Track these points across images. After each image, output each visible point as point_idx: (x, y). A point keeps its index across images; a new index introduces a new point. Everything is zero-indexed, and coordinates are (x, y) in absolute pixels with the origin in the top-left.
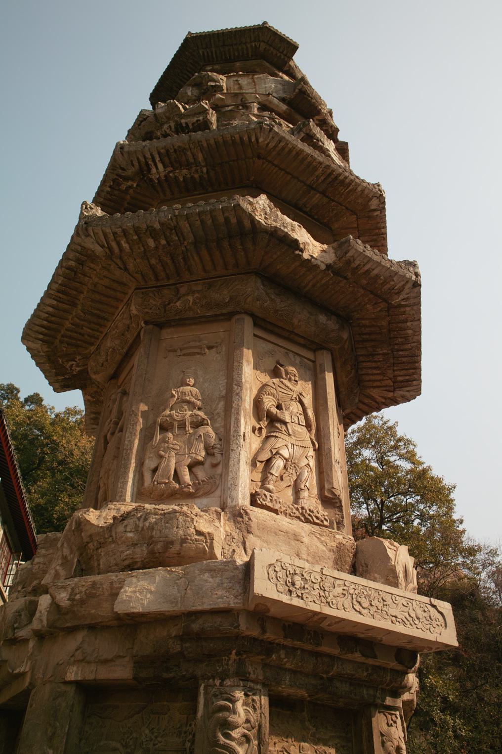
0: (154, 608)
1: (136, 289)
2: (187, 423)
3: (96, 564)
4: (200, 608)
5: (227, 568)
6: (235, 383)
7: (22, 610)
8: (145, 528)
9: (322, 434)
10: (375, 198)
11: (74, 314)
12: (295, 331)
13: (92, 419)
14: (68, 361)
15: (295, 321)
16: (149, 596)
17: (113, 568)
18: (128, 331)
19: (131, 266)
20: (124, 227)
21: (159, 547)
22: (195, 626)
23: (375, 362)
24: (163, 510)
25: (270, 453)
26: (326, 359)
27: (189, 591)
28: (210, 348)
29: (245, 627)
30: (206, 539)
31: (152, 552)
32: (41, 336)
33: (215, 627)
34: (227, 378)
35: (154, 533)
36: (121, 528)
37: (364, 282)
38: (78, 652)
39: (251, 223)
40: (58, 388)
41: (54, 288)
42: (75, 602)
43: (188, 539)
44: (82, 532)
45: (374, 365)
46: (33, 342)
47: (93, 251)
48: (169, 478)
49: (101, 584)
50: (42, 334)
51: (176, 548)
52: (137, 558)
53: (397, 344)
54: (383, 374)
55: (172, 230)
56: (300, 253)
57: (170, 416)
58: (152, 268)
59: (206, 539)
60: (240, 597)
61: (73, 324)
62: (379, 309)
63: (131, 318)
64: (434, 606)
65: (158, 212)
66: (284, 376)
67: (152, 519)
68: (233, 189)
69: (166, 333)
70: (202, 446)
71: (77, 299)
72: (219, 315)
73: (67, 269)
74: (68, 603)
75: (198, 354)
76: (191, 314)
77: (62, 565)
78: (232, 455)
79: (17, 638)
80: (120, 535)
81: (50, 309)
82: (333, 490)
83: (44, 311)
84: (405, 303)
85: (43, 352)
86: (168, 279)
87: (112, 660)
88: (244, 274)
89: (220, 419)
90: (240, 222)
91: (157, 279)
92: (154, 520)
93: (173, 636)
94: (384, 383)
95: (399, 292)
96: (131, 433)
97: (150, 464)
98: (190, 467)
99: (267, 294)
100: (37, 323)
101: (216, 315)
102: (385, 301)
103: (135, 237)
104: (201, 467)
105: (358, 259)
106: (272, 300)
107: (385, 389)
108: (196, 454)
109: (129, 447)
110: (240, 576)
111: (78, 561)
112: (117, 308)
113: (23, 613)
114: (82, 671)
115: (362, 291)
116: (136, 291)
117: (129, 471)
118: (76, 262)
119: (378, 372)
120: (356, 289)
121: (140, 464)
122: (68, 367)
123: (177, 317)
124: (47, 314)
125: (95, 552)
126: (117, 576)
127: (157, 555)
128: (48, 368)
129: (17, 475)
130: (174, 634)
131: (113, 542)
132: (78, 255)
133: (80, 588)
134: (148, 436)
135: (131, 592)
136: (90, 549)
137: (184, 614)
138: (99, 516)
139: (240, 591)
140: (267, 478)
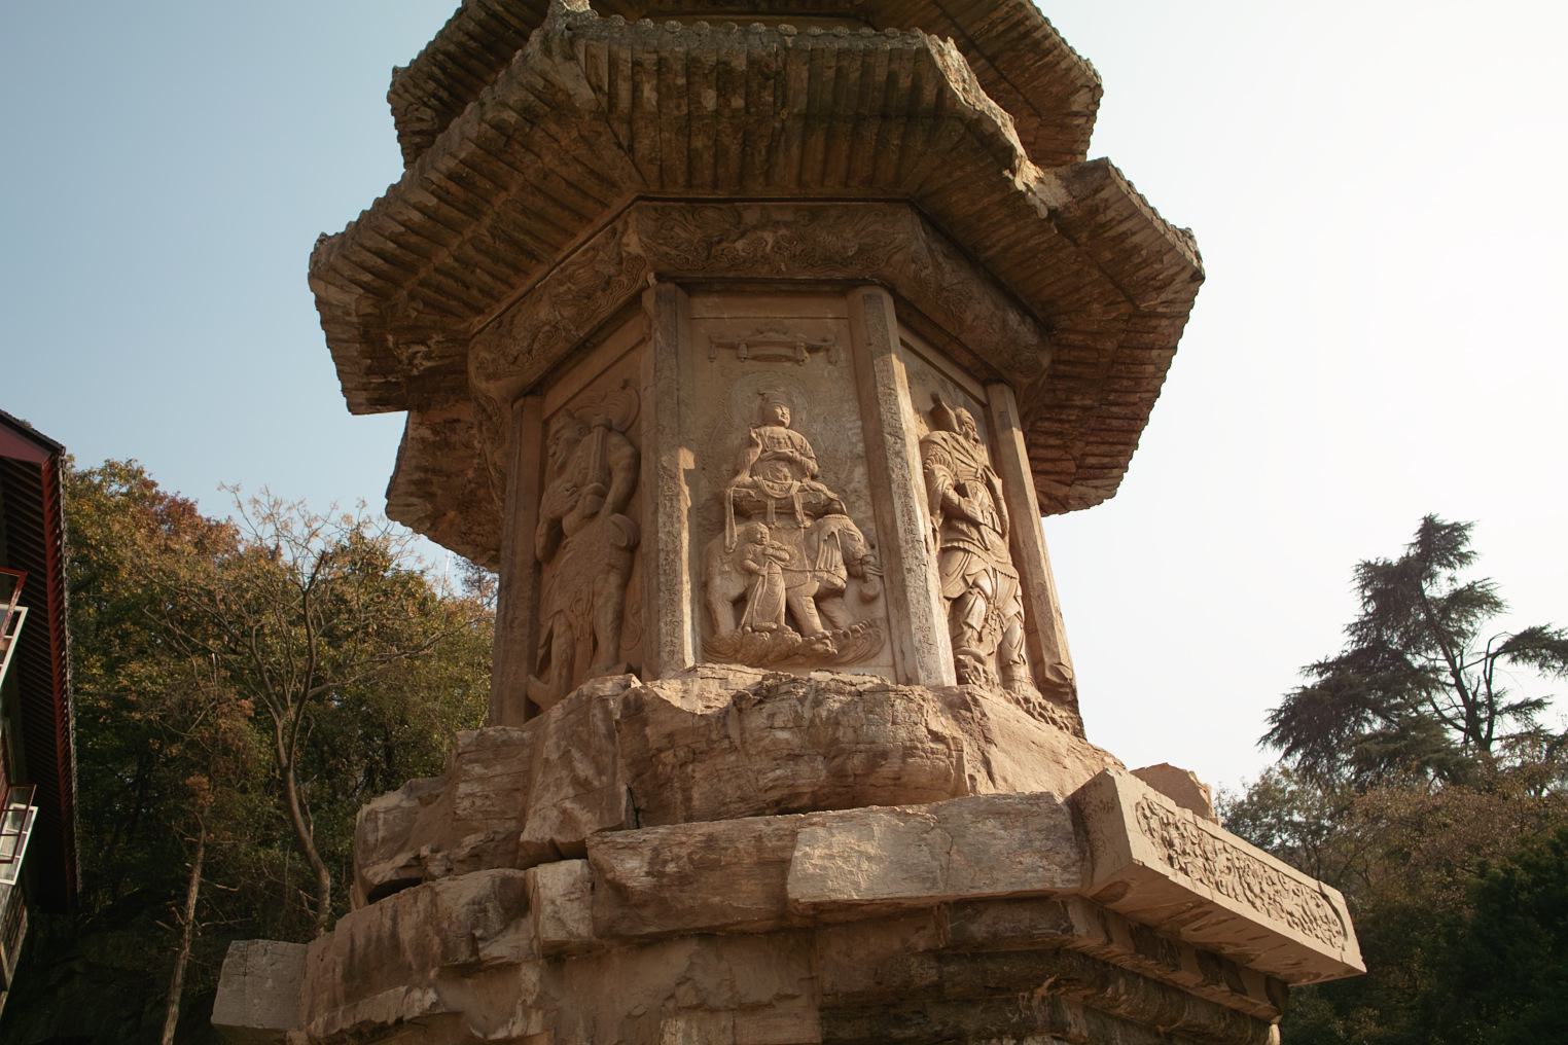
0: (884, 892)
1: (639, 198)
2: (797, 506)
3: (679, 797)
4: (988, 891)
5: (1035, 808)
6: (887, 429)
7: (488, 898)
8: (817, 720)
9: (1024, 555)
10: (1086, 90)
11: (468, 233)
12: (962, 338)
13: (416, 483)
14: (408, 344)
15: (969, 317)
16: (865, 865)
17: (732, 806)
18: (604, 290)
19: (644, 146)
20: (663, 54)
21: (857, 762)
22: (979, 929)
23: (1061, 421)
24: (852, 685)
25: (962, 584)
26: (1006, 403)
27: (955, 857)
28: (812, 350)
29: (1084, 933)
30: (949, 748)
31: (839, 774)
32: (367, 277)
33: (1022, 931)
34: (863, 418)
35: (840, 733)
36: (757, 720)
37: (1108, 255)
38: (683, 988)
39: (938, 94)
40: (360, 404)
41: (443, 168)
42: (665, 880)
43: (917, 748)
44: (646, 725)
45: (1056, 427)
46: (342, 288)
47: (569, 96)
48: (777, 621)
49: (731, 841)
50: (371, 273)
51: (891, 767)
52: (804, 785)
53: (1116, 391)
54: (1065, 448)
55: (767, 79)
56: (1010, 176)
57: (755, 486)
58: (692, 157)
59: (949, 748)
60: (1074, 869)
61: (456, 259)
62: (1114, 315)
63: (621, 263)
64: (1325, 897)
65: (746, 33)
66: (957, 428)
67: (835, 703)
68: (815, 15)
69: (703, 306)
70: (838, 556)
71: (488, 202)
72: (825, 282)
73: (492, 127)
74: (647, 881)
75: (788, 359)
76: (764, 271)
77: (577, 798)
78: (910, 580)
79: (483, 962)
80: (756, 734)
81: (416, 216)
82: (1060, 667)
83: (399, 218)
84: (1164, 310)
85: (358, 316)
86: (715, 185)
87: (769, 1005)
88: (886, 201)
89: (862, 503)
90: (916, 88)
91: (689, 185)
92: (837, 705)
93: (921, 950)
94: (1060, 467)
95: (1161, 289)
96: (670, 516)
97: (726, 586)
98: (818, 599)
99: (930, 251)
100: (369, 244)
101: (818, 282)
102: (1131, 300)
103: (681, 81)
104: (838, 600)
105: (1115, 206)
106: (938, 266)
107: (1057, 478)
108: (828, 572)
109: (670, 547)
110: (1069, 825)
111: (629, 789)
112: (573, 235)
113: (489, 906)
114: (699, 1029)
115: (1096, 274)
116: (639, 203)
117: (681, 600)
118: (520, 115)
119: (1058, 442)
120: (1086, 269)
121: (702, 587)
122: (404, 357)
123: (732, 274)
124: (403, 225)
125: (677, 772)
126: (769, 823)
127: (851, 779)
128: (356, 354)
129: (62, 602)
130: (922, 946)
131: (733, 749)
132: (532, 98)
133: (676, 850)
134: (709, 524)
135: (820, 857)
136: (665, 765)
137: (946, 903)
138: (685, 692)
139: (1072, 855)
140: (963, 633)
